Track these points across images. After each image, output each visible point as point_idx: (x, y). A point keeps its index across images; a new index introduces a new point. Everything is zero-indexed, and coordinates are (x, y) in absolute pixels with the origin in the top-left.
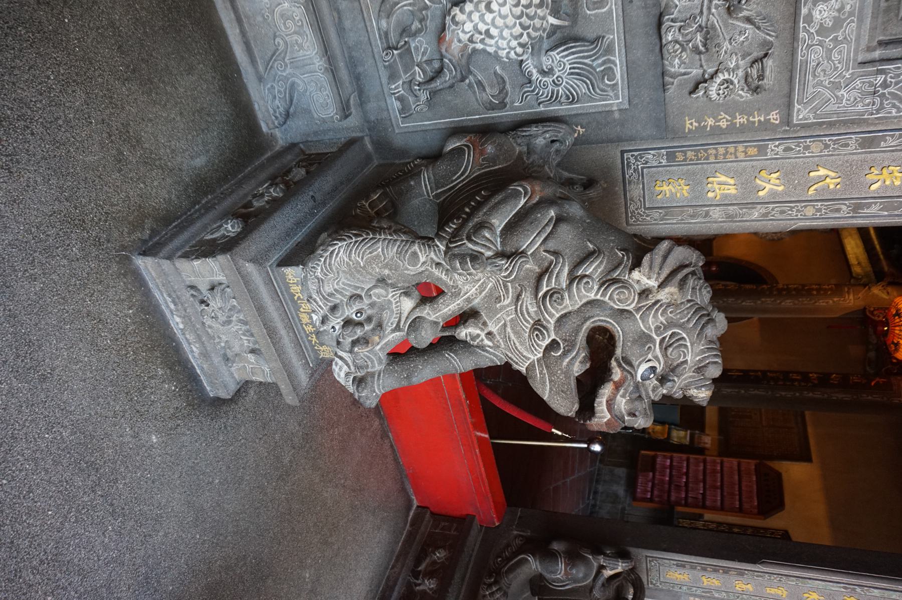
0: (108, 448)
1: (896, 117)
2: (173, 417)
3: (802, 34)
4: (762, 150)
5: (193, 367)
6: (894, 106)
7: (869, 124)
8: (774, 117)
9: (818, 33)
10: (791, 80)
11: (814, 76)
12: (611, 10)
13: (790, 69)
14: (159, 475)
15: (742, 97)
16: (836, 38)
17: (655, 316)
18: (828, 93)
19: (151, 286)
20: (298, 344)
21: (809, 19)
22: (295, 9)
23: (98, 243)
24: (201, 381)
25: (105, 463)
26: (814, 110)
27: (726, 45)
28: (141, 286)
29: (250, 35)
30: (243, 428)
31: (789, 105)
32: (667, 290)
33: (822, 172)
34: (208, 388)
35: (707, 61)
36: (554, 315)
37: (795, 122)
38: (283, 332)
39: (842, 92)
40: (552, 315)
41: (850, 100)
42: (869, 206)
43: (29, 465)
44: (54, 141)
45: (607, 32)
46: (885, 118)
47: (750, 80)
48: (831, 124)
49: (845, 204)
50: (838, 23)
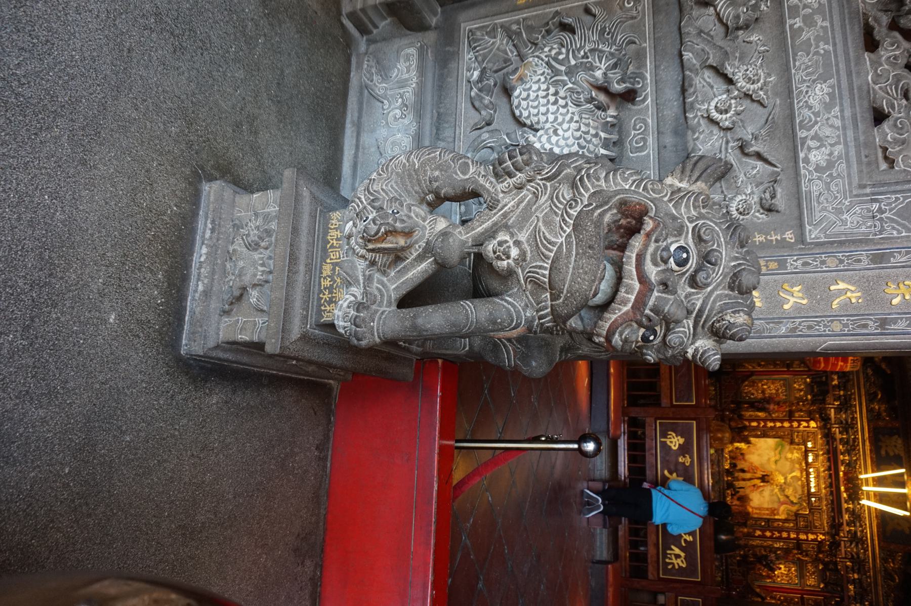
0: (75, 272)
1: (898, 238)
2: (139, 322)
3: (803, 171)
4: (782, 264)
5: (186, 307)
6: (894, 228)
7: (875, 244)
8: (789, 236)
9: (816, 170)
10: (799, 206)
11: (819, 203)
12: (649, 154)
13: (797, 197)
14: (89, 354)
15: (759, 219)
16: (831, 175)
17: (687, 207)
18: (833, 217)
19: (201, 213)
20: (307, 291)
21: (807, 161)
22: (405, 139)
23: (190, 144)
24: (183, 329)
25: (62, 278)
26: (824, 231)
27: (742, 177)
28: (194, 204)
29: (360, 159)
30: (185, 421)
31: (801, 226)
32: (699, 183)
33: (842, 286)
34: (184, 342)
35: (727, 189)
36: (589, 189)
37: (808, 241)
38: (302, 268)
39: (845, 216)
40: (587, 190)
41: (853, 221)
42: (895, 321)
43: (14, 197)
44: (210, 72)
45: (645, 169)
46: (889, 238)
47: (764, 201)
48: (841, 243)
49: (871, 320)
50: (830, 165)
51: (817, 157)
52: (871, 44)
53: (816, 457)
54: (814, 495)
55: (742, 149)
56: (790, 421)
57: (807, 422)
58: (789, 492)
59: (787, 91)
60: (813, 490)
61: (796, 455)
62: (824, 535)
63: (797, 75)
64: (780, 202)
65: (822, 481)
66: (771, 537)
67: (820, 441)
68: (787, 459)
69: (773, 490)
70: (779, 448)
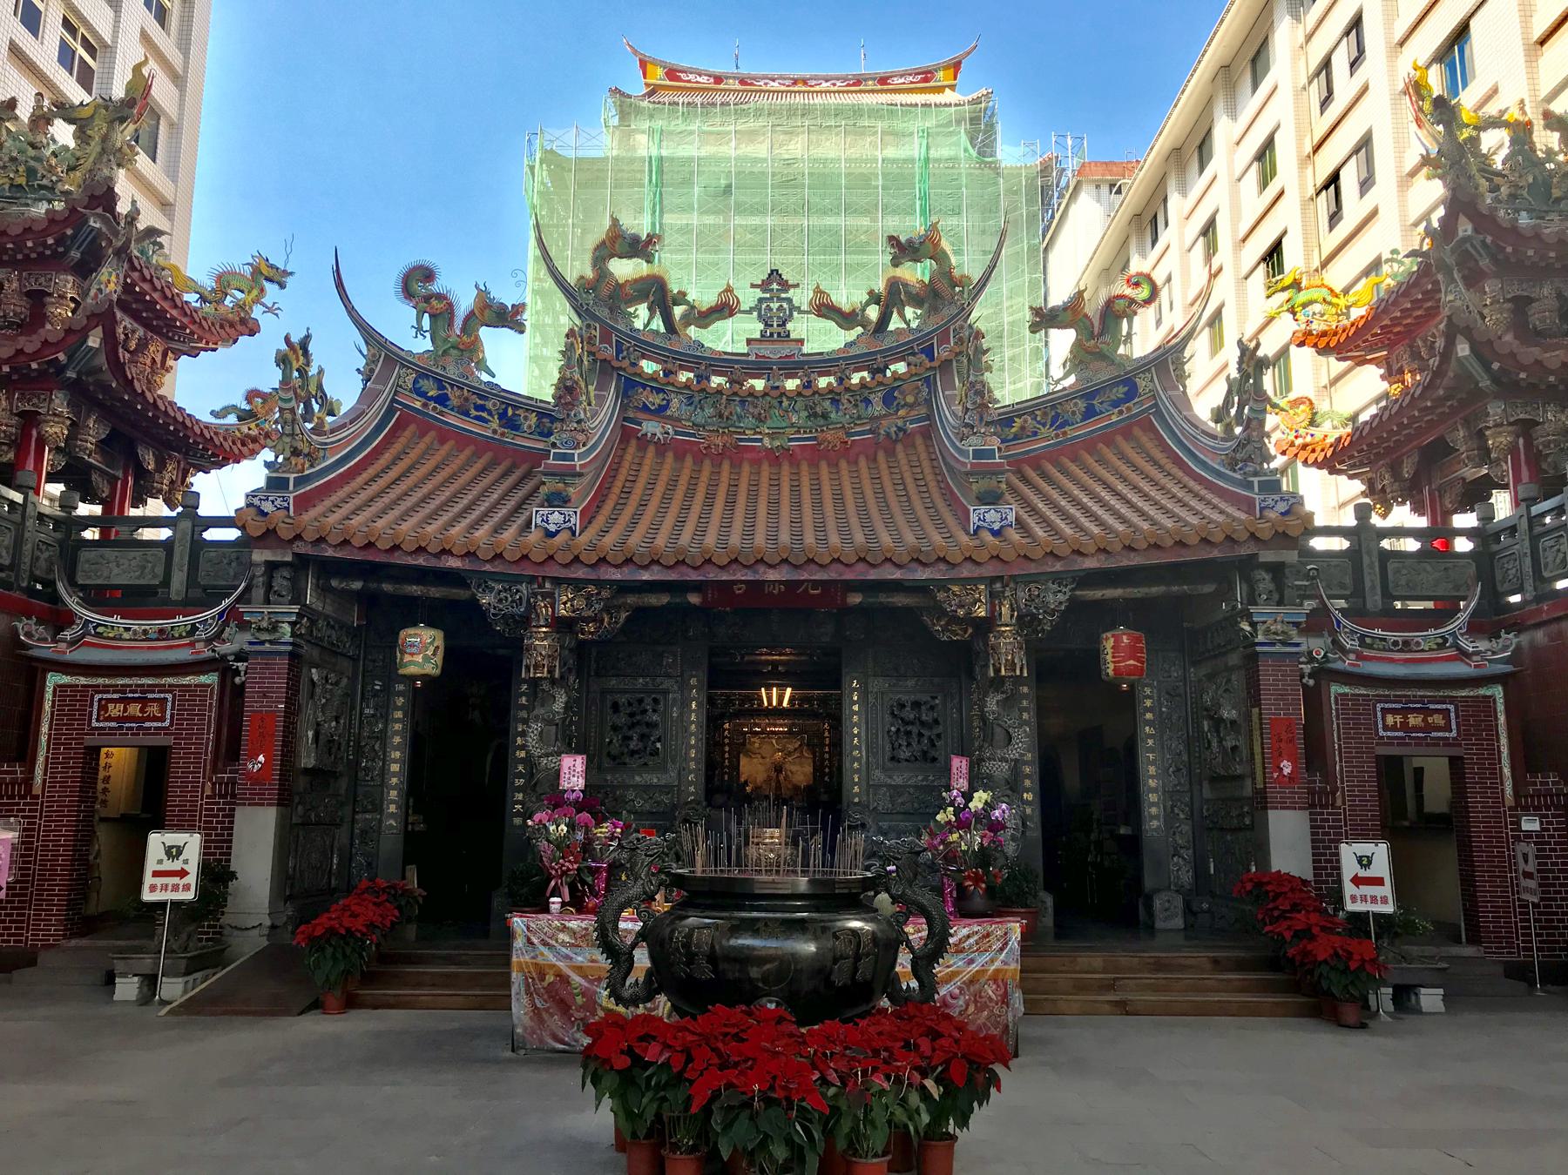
13: (665, 786)
54: (790, 727)
59: (635, 787)
70: (749, 754)
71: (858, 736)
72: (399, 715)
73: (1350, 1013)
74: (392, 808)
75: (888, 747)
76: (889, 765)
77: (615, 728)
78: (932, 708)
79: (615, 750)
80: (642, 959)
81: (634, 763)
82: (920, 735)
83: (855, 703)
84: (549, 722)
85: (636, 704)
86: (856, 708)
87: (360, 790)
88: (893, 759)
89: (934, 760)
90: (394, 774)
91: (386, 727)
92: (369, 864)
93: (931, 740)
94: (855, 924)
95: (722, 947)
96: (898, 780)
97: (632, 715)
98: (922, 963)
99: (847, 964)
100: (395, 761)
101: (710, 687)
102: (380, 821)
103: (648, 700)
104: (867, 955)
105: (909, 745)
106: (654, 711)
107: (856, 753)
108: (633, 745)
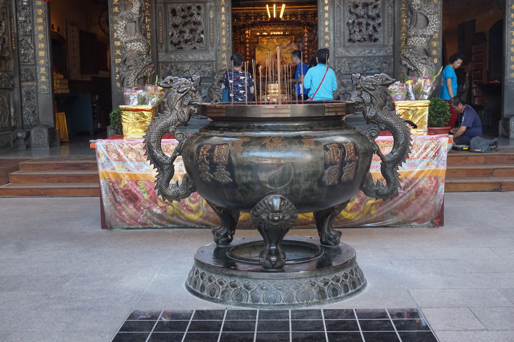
13: (208, 61)
41: (213, 54)
51: (202, 58)
52: (182, 48)
53: (264, 31)
54: (284, 33)
55: (199, 69)
56: (246, 43)
57: (246, 35)
58: (285, 44)
59: (189, 62)
60: (282, 33)
61: (265, 40)
62: (304, 29)
63: (187, 60)
64: (209, 64)
65: (277, 29)
66: (308, 55)
67: (256, 29)
68: (267, 45)
69: (285, 53)
70: (261, 49)
71: (328, 26)
72: (40, 20)
73: (110, 132)
74: (43, 79)
75: (347, 32)
76: (348, 44)
77: (175, 26)
78: (375, 7)
79: (175, 40)
80: (180, 168)
81: (187, 47)
82: (368, 24)
83: (326, 5)
84: (131, 20)
85: (186, 10)
86: (327, 8)
87: (23, 68)
88: (350, 40)
89: (376, 40)
90: (42, 58)
91: (33, 27)
92: (34, 112)
93: (374, 28)
94: (341, 139)
95: (237, 160)
96: (353, 53)
97: (184, 17)
98: (390, 166)
99: (334, 169)
100: (41, 50)
101: (233, 5)
102: (37, 87)
103: (194, 7)
104: (350, 161)
105: (360, 31)
106: (198, 14)
107: (327, 37)
108: (187, 36)
